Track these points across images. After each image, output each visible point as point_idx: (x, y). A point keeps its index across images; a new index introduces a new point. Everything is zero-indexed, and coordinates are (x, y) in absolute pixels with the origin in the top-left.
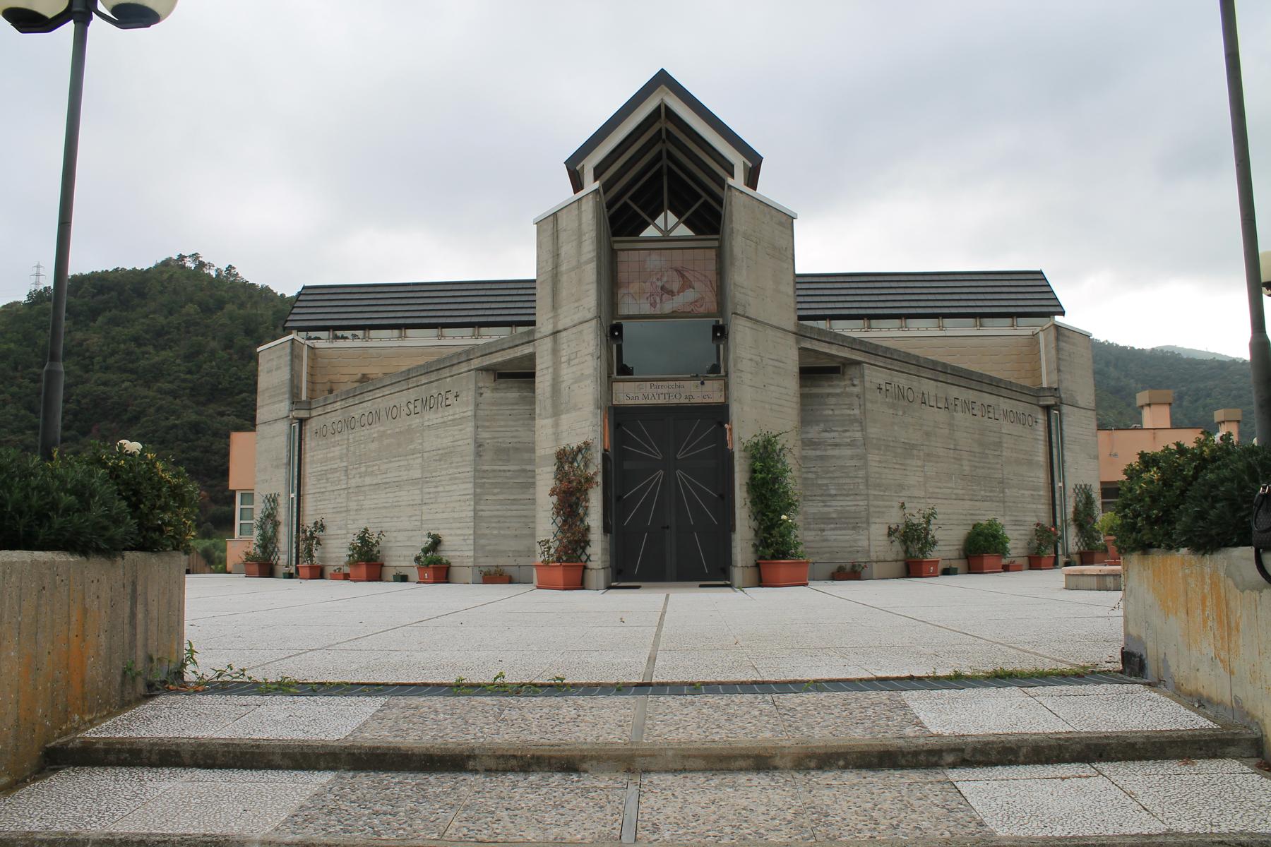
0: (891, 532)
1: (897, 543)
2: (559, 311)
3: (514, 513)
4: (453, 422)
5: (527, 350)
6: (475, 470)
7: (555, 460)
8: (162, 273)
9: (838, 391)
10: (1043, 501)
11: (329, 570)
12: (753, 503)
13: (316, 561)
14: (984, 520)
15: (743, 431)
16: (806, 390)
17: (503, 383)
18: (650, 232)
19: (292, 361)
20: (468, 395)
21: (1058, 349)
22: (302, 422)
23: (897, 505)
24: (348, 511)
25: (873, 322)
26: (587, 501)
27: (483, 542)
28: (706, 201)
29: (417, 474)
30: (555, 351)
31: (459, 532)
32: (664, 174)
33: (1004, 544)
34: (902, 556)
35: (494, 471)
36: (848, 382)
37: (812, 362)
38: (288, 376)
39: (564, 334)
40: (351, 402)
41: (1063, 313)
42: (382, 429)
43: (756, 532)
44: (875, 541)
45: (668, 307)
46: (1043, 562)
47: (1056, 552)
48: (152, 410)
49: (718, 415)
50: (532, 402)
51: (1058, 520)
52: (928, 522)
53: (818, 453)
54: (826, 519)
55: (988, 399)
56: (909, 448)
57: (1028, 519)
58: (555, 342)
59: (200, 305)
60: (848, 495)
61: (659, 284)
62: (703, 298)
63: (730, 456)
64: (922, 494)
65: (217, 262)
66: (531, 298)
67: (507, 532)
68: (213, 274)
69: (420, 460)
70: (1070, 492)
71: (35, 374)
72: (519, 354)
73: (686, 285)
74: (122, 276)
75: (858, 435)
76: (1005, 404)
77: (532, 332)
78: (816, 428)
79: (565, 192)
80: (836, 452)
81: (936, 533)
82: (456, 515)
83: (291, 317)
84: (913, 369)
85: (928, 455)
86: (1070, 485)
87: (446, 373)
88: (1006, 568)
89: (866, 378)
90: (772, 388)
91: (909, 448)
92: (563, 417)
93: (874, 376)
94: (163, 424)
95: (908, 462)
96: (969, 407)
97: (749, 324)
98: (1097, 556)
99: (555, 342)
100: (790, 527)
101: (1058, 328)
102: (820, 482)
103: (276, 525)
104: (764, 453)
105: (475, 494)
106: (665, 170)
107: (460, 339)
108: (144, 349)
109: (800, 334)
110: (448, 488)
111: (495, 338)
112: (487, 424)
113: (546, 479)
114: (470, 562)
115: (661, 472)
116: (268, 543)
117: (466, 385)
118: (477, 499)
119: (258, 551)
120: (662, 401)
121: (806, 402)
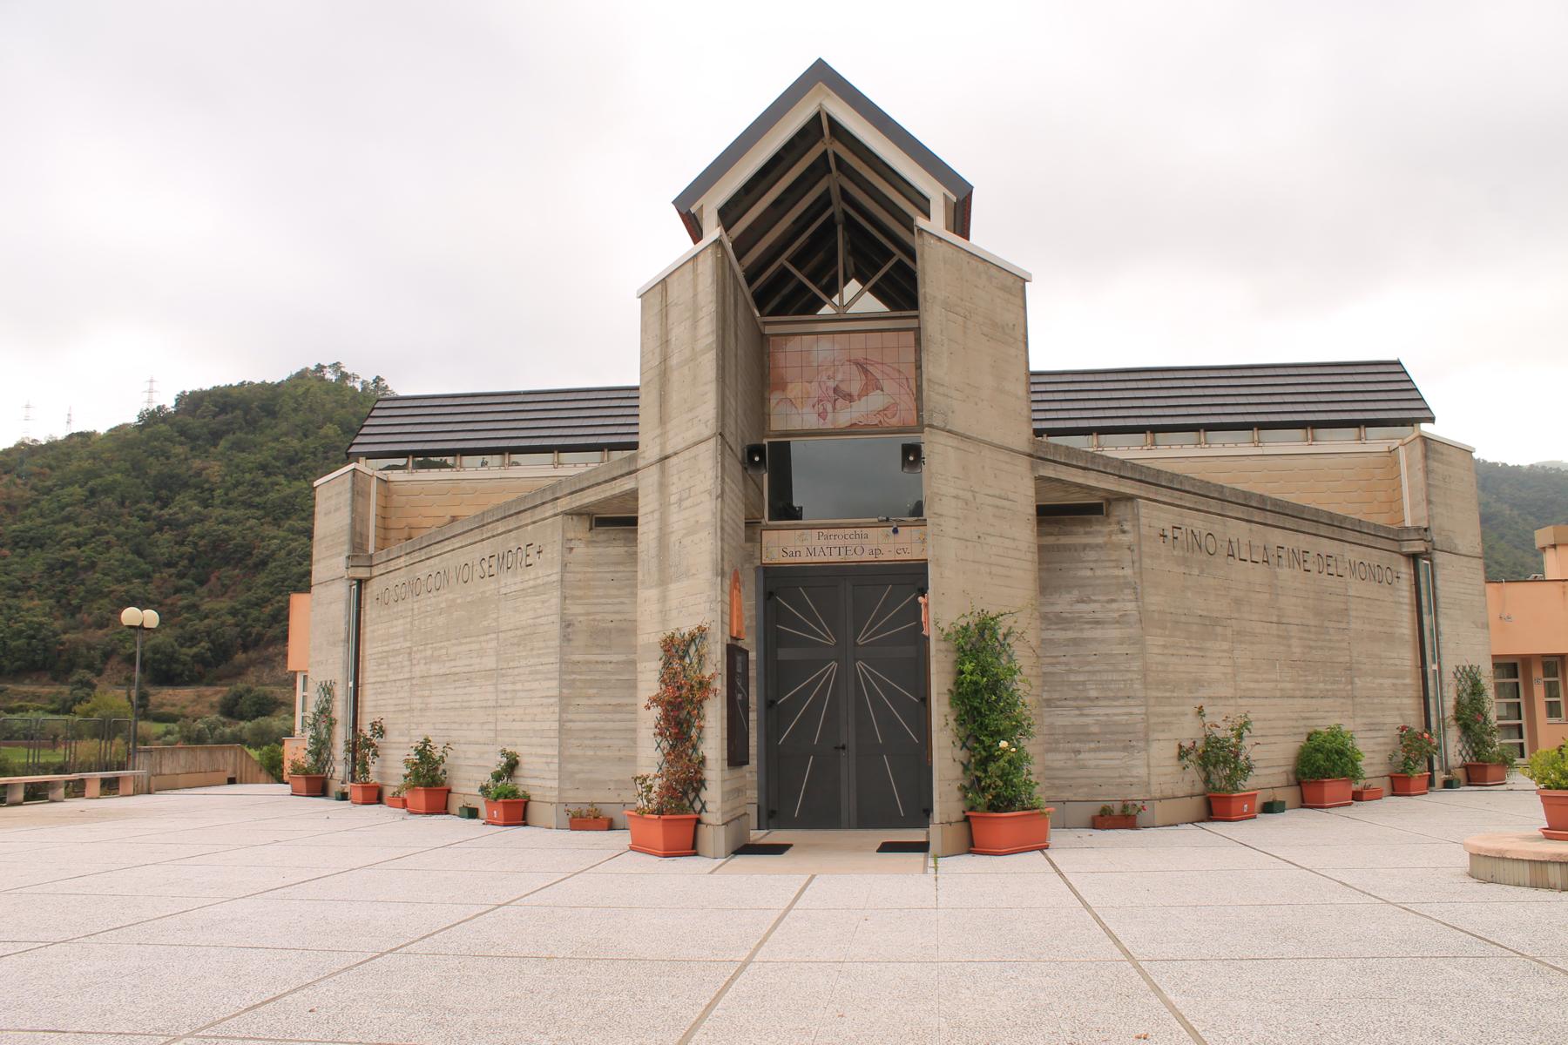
0: (1182, 754)
1: (1192, 768)
2: (669, 426)
3: (617, 725)
4: (530, 592)
5: (626, 485)
6: (562, 661)
7: (660, 653)
8: (296, 386)
9: (1100, 540)
10: (1411, 692)
11: (388, 792)
12: (961, 721)
13: (373, 778)
14: (1323, 724)
15: (943, 611)
16: (1050, 540)
17: (602, 534)
18: (826, 310)
19: (353, 500)
20: (553, 552)
21: (1427, 472)
22: (361, 583)
23: (1191, 710)
24: (411, 710)
25: (1159, 436)
26: (702, 718)
27: (572, 767)
28: (900, 261)
29: (490, 662)
30: (663, 486)
31: (540, 751)
32: (823, 219)
33: (1353, 762)
34: (1199, 787)
35: (588, 662)
36: (1115, 527)
37: (1056, 498)
38: (348, 521)
39: (673, 460)
40: (417, 556)
41: (1432, 420)
42: (451, 596)
43: (966, 768)
44: (1158, 768)
45: (844, 418)
46: (1413, 784)
47: (1431, 768)
48: (283, 553)
49: (914, 577)
50: (633, 557)
51: (1433, 720)
52: (1240, 736)
53: (1070, 634)
54: (1082, 735)
55: (1327, 547)
56: (1210, 624)
57: (1389, 720)
58: (663, 472)
59: (341, 425)
60: (1115, 698)
61: (831, 384)
62: (895, 404)
63: (921, 643)
64: (1230, 692)
65: (363, 372)
66: (633, 402)
67: (605, 753)
68: (359, 387)
69: (494, 644)
70: (1448, 678)
71: (144, 510)
72: (617, 491)
73: (872, 385)
74: (249, 391)
75: (1131, 606)
76: (1352, 554)
77: (633, 459)
78: (1067, 597)
79: (682, 244)
80: (1098, 633)
81: (1251, 750)
82: (537, 726)
83: (359, 439)
84: (1214, 506)
85: (1238, 633)
86: (1449, 666)
87: (527, 518)
88: (1358, 797)
89: (1143, 520)
90: (991, 540)
91: (1210, 624)
92: (672, 586)
93: (1154, 517)
94: (295, 570)
95: (1209, 644)
96: (1299, 558)
97: (952, 441)
98: (1492, 771)
99: (663, 472)
100: (1015, 764)
101: (1425, 440)
102: (1072, 678)
103: (332, 723)
104: (979, 642)
105: (561, 697)
106: (839, 217)
107: (535, 470)
108: (274, 479)
109: (1037, 457)
110: (527, 686)
111: (582, 469)
112: (578, 593)
113: (649, 681)
114: (553, 796)
115: (834, 664)
116: (321, 747)
117: (550, 533)
118: (564, 703)
119: (311, 759)
120: (835, 558)
121: (1046, 555)
